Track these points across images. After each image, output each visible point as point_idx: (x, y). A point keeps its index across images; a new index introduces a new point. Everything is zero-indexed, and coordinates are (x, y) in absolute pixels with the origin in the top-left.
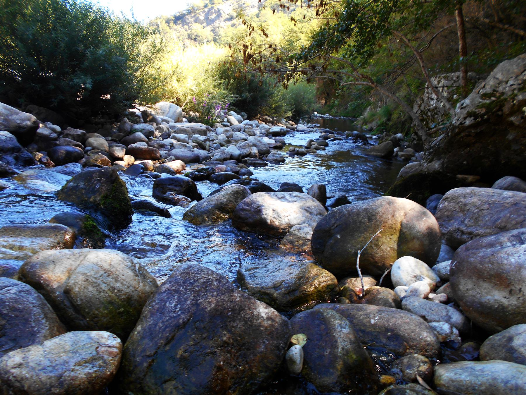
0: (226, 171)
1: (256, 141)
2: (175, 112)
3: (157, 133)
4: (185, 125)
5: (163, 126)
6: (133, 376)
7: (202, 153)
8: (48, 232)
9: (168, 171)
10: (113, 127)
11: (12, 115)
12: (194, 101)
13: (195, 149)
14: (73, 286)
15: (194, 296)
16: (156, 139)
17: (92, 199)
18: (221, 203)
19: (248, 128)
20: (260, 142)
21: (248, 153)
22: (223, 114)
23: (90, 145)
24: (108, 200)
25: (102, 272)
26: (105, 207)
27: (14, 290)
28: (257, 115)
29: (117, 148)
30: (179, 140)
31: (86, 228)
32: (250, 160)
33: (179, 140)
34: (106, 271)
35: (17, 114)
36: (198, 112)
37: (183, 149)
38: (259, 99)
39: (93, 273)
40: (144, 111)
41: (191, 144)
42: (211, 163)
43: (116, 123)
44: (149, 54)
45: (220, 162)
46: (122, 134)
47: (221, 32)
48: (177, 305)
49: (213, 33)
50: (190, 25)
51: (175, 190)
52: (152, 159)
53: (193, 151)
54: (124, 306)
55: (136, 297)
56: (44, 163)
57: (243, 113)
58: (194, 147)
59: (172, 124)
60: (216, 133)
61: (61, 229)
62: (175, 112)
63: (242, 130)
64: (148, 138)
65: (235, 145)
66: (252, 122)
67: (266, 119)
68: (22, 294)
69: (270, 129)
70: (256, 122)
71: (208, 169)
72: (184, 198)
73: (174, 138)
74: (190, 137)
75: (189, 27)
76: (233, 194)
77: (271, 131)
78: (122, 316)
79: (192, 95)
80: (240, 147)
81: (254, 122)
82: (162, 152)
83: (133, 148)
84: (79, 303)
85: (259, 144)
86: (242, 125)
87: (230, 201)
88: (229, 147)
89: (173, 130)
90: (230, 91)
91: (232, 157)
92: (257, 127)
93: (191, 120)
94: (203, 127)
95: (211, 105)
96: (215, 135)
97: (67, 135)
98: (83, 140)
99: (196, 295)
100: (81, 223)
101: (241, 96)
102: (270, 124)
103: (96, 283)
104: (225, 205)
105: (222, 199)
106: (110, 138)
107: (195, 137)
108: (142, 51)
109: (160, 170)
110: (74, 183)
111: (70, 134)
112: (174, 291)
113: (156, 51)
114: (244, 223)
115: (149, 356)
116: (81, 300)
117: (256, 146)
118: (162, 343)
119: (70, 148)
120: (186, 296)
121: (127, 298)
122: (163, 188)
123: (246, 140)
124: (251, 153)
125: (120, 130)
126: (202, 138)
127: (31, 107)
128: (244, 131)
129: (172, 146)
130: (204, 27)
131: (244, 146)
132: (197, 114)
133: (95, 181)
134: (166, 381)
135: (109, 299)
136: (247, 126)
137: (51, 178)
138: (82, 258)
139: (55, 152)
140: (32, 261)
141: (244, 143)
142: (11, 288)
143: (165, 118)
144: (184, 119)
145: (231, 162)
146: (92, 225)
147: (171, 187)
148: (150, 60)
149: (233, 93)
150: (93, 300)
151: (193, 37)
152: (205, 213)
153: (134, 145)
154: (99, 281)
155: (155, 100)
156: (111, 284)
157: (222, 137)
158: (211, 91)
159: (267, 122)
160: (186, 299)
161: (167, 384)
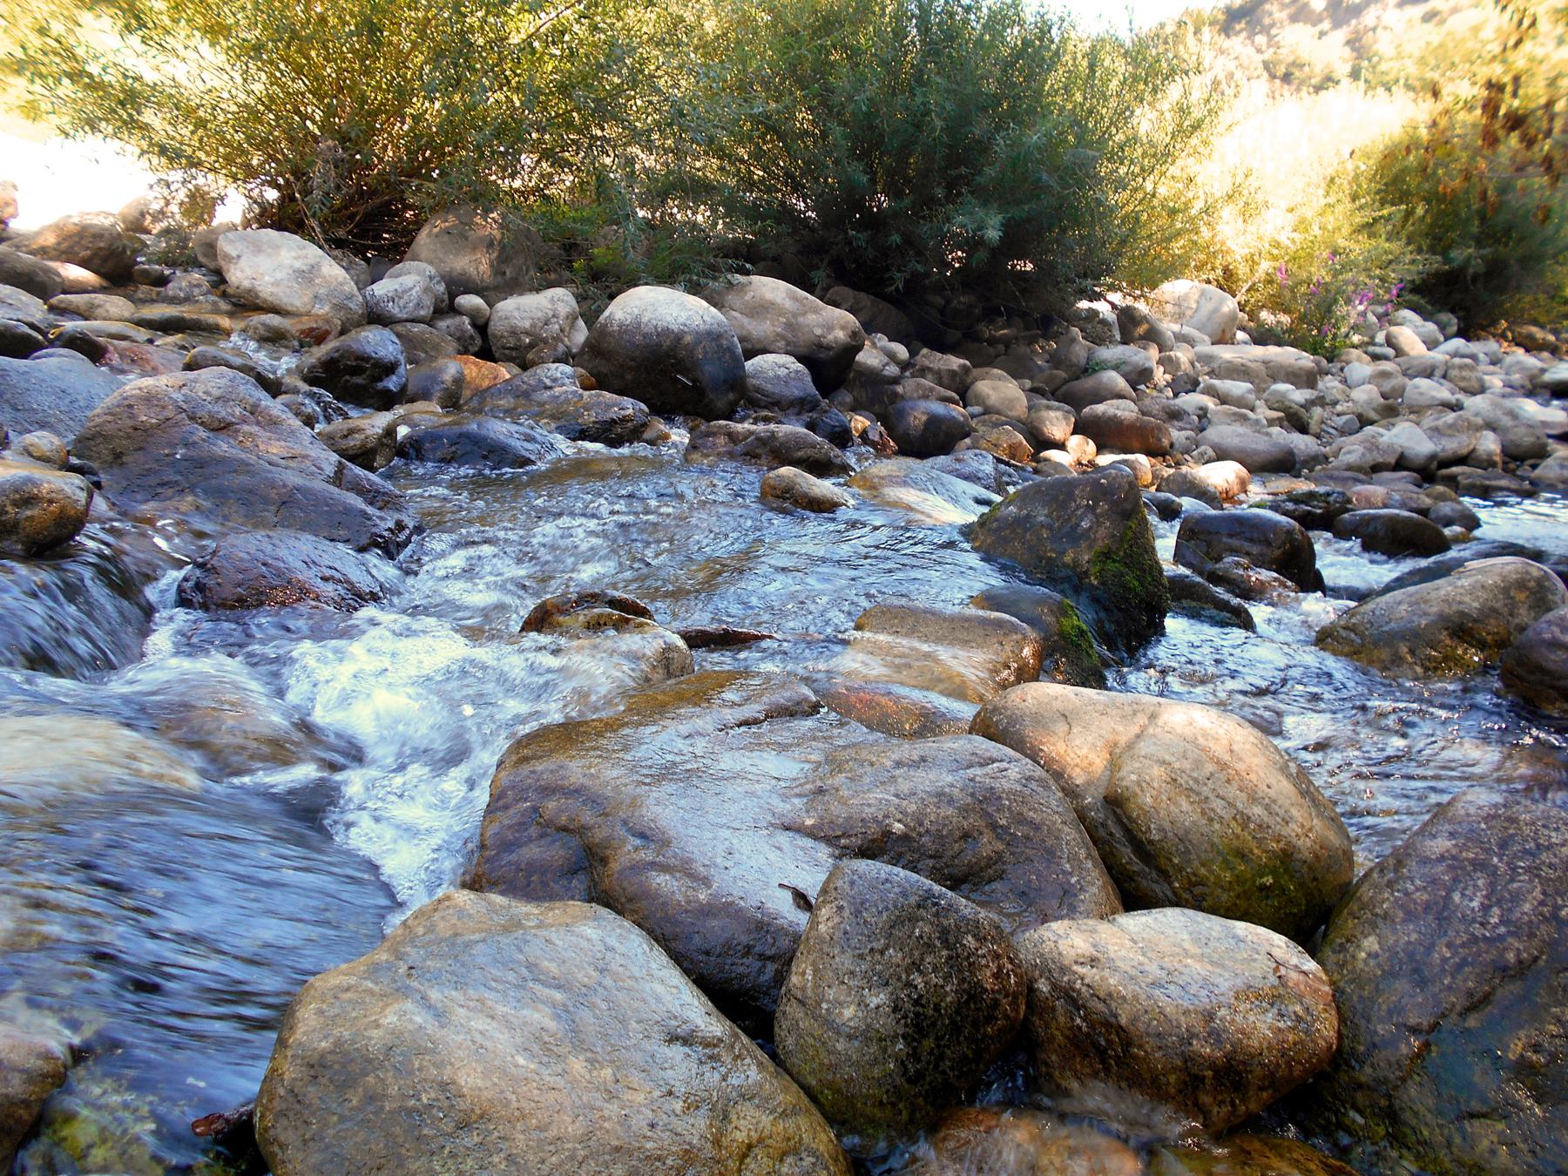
0: (1385, 506)
1: (1499, 413)
2: (1216, 310)
3: (1161, 376)
4: (1246, 352)
5: (1179, 354)
6: (1368, 1070)
7: (1302, 443)
8: (982, 632)
9: (1202, 493)
10: (1034, 352)
11: (804, 314)
12: (1279, 277)
13: (1276, 430)
14: (1138, 790)
15: (1544, 893)
16: (1155, 393)
17: (1068, 558)
18: (1462, 614)
19: (1461, 367)
20: (1513, 415)
21: (1464, 451)
22: (1372, 318)
23: (980, 400)
24: (1111, 566)
25: (1210, 768)
26: (1103, 583)
27: (1014, 772)
28: (1494, 323)
29: (1052, 414)
30: (1223, 399)
31: (1062, 634)
32: (1470, 476)
33: (1223, 399)
34: (1223, 766)
35: (816, 311)
36: (1286, 311)
37: (1239, 429)
38: (1515, 268)
39: (1187, 765)
40: (1128, 307)
41: (1263, 413)
42: (1331, 478)
43: (1042, 342)
44: (1162, 138)
45: (1361, 476)
46: (1062, 374)
47: (1383, 45)
48: (1490, 906)
49: (1353, 50)
50: (1273, 31)
51: (1248, 554)
52: (1150, 453)
53: (1268, 434)
54: (1274, 872)
55: (1307, 855)
56: (873, 444)
57: (1445, 317)
58: (1271, 422)
59: (1206, 348)
60: (1344, 381)
61: (1014, 629)
62: (1216, 310)
63: (1438, 373)
64: (1135, 390)
65: (1418, 424)
66: (1474, 347)
67: (1530, 337)
68: (1033, 785)
69: (1543, 371)
70: (1492, 345)
71: (1328, 494)
72: (1275, 580)
73: (1211, 392)
74: (1259, 390)
75: (1271, 38)
76: (1505, 591)
77: (1547, 377)
78: (1267, 897)
79: (1275, 258)
80: (1436, 430)
81: (1482, 348)
82: (1177, 435)
83: (1096, 416)
84: (1155, 836)
85: (1506, 421)
86: (1439, 356)
87: (1494, 610)
88: (1395, 430)
89: (1206, 369)
90: (1408, 244)
91: (1401, 463)
92: (1493, 363)
93: (1262, 337)
94: (1305, 360)
95: (1339, 291)
96: (1340, 386)
97: (923, 372)
98: (962, 390)
99: (1550, 891)
100: (1050, 619)
101: (1447, 261)
102: (1545, 355)
103: (1198, 794)
104: (1475, 621)
105: (1467, 599)
106: (1028, 384)
107: (1276, 392)
108: (1142, 132)
109: (1174, 487)
110: (1020, 509)
111: (930, 369)
112: (1473, 862)
113: (1188, 127)
114: (1553, 687)
115: (1415, 1030)
116: (1161, 829)
117: (1494, 430)
118: (1453, 1005)
119: (938, 408)
120: (1515, 885)
121: (1283, 851)
122: (1209, 544)
123: (1455, 407)
124: (1474, 450)
125: (1056, 360)
126: (1298, 396)
127: (840, 291)
128: (1444, 377)
129: (1203, 413)
130: (1322, 34)
131: (1451, 426)
132: (1285, 319)
133: (1078, 507)
134: (1473, 1116)
135: (1235, 843)
136: (1457, 361)
137: (939, 488)
138: (1142, 719)
139: (902, 414)
140: (1009, 704)
141: (1451, 417)
142: (1005, 765)
143: (1187, 330)
144: (1241, 335)
145: (1399, 479)
146: (1079, 627)
147: (1235, 542)
148: (1166, 156)
149: (1420, 251)
150: (1194, 837)
151: (1281, 70)
152: (1403, 638)
153: (1100, 408)
154: (1205, 791)
155: (1148, 277)
156: (1240, 806)
157: (1365, 395)
158: (1341, 242)
159: (1531, 346)
160: (1516, 898)
161: (1476, 1123)
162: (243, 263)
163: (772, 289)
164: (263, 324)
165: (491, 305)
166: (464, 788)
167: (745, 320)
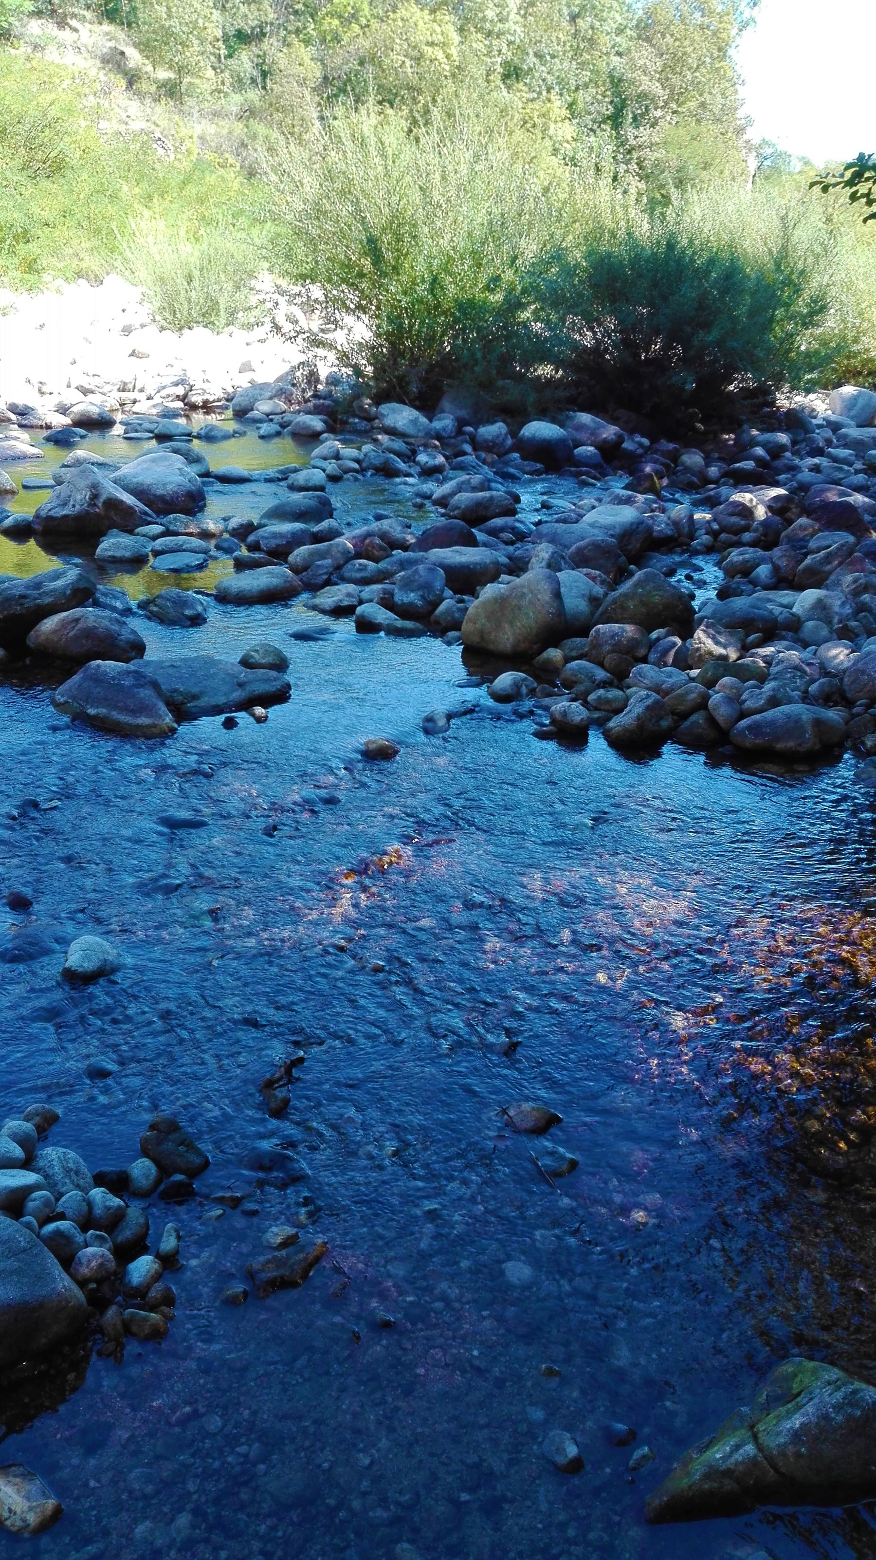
23: (683, 464)
162: (390, 417)
163: (585, 418)
164: (782, 713)
165: (476, 430)
166: (544, 774)
167: (574, 432)
